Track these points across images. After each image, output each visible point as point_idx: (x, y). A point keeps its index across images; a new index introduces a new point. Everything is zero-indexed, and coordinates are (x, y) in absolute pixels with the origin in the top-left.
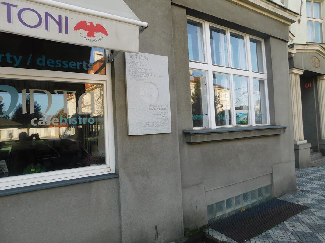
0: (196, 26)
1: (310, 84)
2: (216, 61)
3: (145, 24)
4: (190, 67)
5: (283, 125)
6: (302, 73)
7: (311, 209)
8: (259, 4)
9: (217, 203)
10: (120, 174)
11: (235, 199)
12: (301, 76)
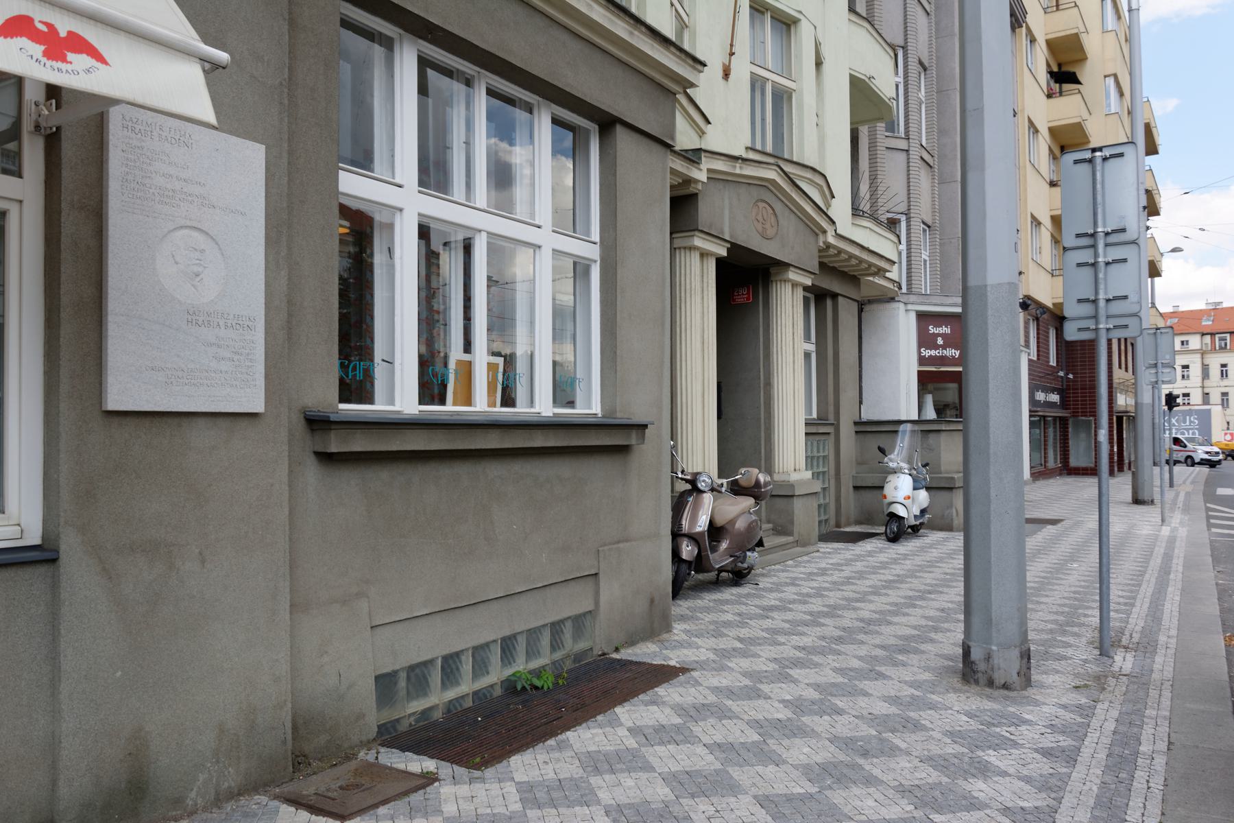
0: (373, 41)
1: (748, 293)
2: (433, 174)
3: (223, 56)
4: (341, 189)
5: (638, 419)
6: (724, 253)
7: (695, 674)
8: (584, 9)
9: (411, 668)
10: (63, 548)
11: (473, 656)
12: (720, 262)
